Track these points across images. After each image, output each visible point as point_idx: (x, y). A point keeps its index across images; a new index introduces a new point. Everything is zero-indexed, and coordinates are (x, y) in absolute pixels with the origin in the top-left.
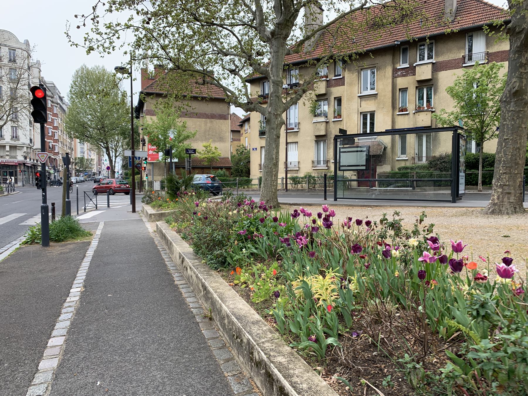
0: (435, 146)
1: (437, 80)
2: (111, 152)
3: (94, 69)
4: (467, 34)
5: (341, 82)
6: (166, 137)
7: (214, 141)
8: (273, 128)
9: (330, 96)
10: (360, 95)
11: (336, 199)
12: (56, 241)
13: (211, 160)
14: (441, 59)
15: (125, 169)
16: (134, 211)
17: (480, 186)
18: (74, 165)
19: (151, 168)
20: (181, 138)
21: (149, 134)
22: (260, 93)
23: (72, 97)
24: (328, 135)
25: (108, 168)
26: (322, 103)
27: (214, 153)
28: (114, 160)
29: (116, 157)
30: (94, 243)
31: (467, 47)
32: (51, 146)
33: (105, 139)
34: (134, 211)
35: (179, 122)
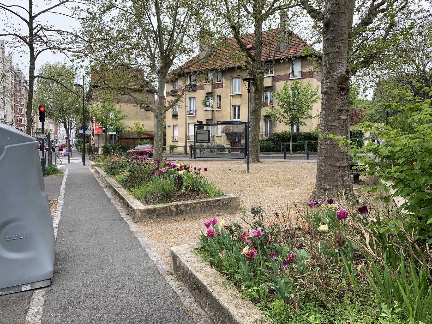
0: (274, 127)
1: (275, 87)
2: (67, 125)
3: (55, 65)
4: (291, 60)
5: (221, 85)
6: (107, 118)
7: (143, 120)
8: (159, 121)
9: (214, 94)
10: (232, 94)
11: (195, 158)
12: (47, 175)
13: (139, 133)
14: (277, 74)
15: (78, 138)
16: (84, 164)
17: (291, 152)
18: (36, 134)
19: (97, 138)
20: (118, 118)
21: (96, 115)
22: (172, 89)
23: (38, 85)
24: (214, 118)
25: (66, 138)
26: (210, 98)
27: (141, 128)
28: (69, 131)
29: (71, 129)
30: (66, 176)
31: (291, 67)
32: (19, 120)
33: (64, 116)
34: (84, 164)
35: (117, 106)
